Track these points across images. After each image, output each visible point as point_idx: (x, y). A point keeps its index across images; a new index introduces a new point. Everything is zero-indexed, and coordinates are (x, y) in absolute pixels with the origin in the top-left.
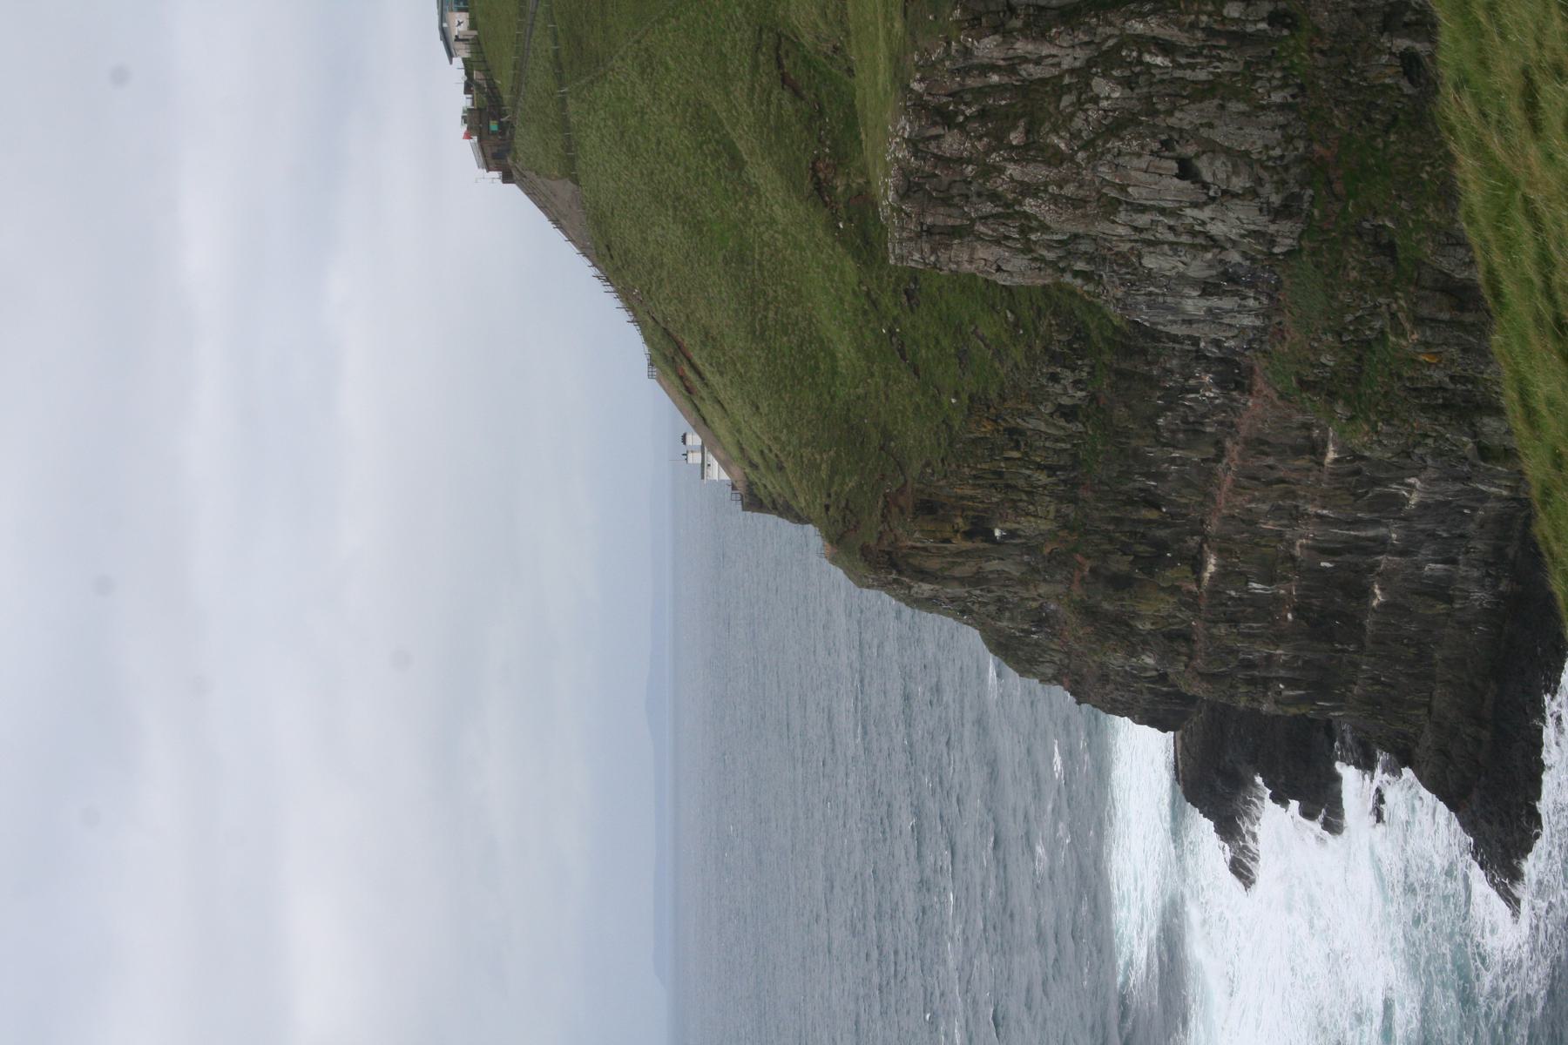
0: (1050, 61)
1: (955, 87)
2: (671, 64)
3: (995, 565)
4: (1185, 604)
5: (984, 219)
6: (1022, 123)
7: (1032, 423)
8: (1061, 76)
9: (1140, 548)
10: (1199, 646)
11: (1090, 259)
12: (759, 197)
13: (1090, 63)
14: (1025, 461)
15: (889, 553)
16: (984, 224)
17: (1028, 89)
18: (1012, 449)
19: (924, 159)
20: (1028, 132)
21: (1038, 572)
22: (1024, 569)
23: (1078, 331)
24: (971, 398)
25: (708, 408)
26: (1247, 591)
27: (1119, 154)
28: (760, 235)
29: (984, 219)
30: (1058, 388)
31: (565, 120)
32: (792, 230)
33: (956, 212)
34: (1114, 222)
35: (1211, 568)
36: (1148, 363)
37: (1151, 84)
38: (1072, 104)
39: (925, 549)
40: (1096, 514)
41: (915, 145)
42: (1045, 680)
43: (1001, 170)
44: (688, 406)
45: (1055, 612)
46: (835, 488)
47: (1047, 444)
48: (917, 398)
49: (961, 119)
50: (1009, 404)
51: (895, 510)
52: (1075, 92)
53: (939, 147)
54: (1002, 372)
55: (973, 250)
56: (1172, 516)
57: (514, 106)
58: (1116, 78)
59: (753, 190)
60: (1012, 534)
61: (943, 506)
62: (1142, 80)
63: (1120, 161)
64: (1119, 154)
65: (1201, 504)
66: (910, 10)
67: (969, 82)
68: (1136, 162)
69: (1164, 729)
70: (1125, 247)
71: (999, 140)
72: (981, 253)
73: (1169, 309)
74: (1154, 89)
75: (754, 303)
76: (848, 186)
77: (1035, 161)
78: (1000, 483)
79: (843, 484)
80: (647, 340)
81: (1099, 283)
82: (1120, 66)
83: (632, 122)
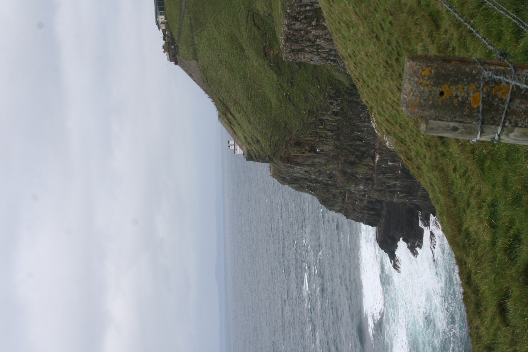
3: (317, 160)
4: (371, 169)
5: (307, 46)
6: (315, 20)
7: (326, 118)
9: (357, 153)
10: (375, 181)
11: (334, 57)
14: (324, 129)
15: (287, 158)
20: (317, 22)
23: (337, 90)
24: (309, 111)
25: (236, 128)
26: (387, 165)
29: (307, 46)
30: (332, 107)
31: (194, 42)
33: (300, 45)
35: (377, 159)
36: (357, 98)
39: (297, 156)
42: (337, 212)
43: (311, 32)
44: (230, 129)
45: (335, 174)
46: (272, 140)
48: (294, 112)
50: (319, 112)
51: (289, 145)
54: (317, 103)
55: (305, 55)
56: (366, 143)
57: (178, 40)
59: (247, 58)
60: (322, 151)
61: (302, 143)
65: (374, 139)
69: (373, 226)
71: (310, 24)
72: (306, 56)
76: (274, 53)
80: (218, 109)
81: (337, 63)
83: (213, 41)
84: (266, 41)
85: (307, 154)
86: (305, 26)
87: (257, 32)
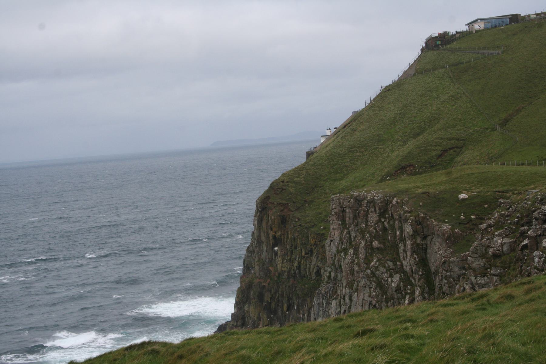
0: (405, 256)
1: (395, 217)
2: (454, 107)
5: (349, 233)
6: (381, 246)
8: (400, 261)
9: (273, 305)
11: (335, 278)
12: (402, 146)
13: (405, 272)
16: (347, 233)
17: (395, 247)
18: (305, 252)
19: (367, 206)
20: (378, 248)
21: (263, 265)
22: (264, 260)
24: (323, 234)
27: (370, 288)
28: (388, 147)
31: (437, 69)
32: (389, 159)
33: (351, 221)
34: (346, 287)
37: (398, 299)
38: (389, 266)
39: (268, 221)
40: (284, 287)
41: (372, 202)
46: (290, 184)
47: (308, 265)
49: (383, 220)
51: (282, 208)
52: (394, 267)
53: (371, 212)
55: (337, 230)
56: (285, 316)
58: (400, 284)
59: (405, 143)
60: (276, 254)
62: (399, 295)
63: (367, 288)
64: (370, 288)
66: (424, 195)
67: (396, 222)
68: (367, 295)
70: (339, 293)
71: (374, 237)
72: (337, 233)
73: (318, 313)
74: (396, 300)
75: (362, 147)
77: (366, 253)
78: (293, 248)
79: (292, 187)
81: (328, 283)
82: (404, 286)
84: (421, 167)
85: (271, 234)
86: (372, 229)
87: (434, 154)
